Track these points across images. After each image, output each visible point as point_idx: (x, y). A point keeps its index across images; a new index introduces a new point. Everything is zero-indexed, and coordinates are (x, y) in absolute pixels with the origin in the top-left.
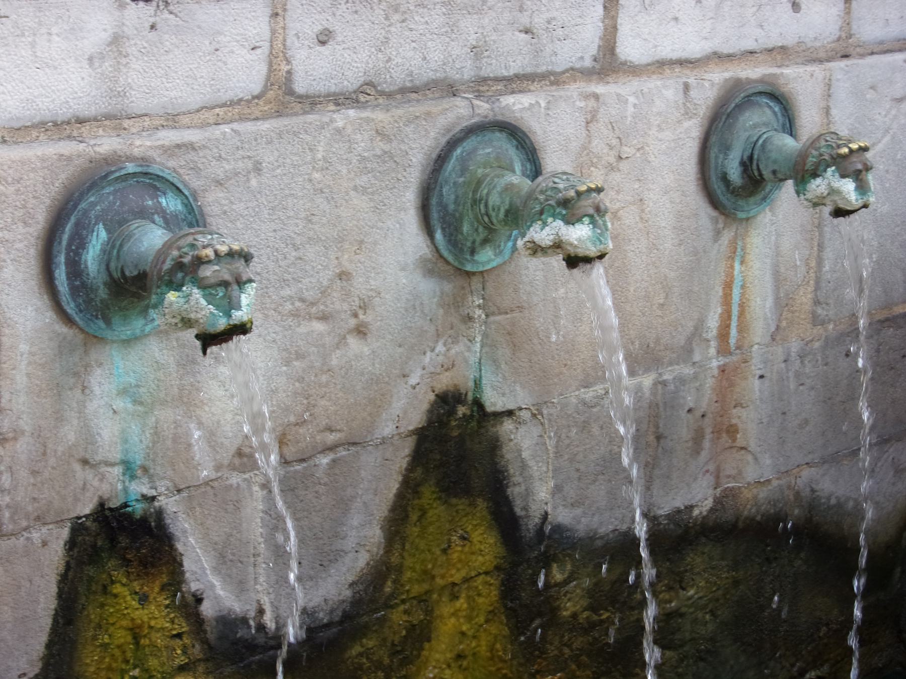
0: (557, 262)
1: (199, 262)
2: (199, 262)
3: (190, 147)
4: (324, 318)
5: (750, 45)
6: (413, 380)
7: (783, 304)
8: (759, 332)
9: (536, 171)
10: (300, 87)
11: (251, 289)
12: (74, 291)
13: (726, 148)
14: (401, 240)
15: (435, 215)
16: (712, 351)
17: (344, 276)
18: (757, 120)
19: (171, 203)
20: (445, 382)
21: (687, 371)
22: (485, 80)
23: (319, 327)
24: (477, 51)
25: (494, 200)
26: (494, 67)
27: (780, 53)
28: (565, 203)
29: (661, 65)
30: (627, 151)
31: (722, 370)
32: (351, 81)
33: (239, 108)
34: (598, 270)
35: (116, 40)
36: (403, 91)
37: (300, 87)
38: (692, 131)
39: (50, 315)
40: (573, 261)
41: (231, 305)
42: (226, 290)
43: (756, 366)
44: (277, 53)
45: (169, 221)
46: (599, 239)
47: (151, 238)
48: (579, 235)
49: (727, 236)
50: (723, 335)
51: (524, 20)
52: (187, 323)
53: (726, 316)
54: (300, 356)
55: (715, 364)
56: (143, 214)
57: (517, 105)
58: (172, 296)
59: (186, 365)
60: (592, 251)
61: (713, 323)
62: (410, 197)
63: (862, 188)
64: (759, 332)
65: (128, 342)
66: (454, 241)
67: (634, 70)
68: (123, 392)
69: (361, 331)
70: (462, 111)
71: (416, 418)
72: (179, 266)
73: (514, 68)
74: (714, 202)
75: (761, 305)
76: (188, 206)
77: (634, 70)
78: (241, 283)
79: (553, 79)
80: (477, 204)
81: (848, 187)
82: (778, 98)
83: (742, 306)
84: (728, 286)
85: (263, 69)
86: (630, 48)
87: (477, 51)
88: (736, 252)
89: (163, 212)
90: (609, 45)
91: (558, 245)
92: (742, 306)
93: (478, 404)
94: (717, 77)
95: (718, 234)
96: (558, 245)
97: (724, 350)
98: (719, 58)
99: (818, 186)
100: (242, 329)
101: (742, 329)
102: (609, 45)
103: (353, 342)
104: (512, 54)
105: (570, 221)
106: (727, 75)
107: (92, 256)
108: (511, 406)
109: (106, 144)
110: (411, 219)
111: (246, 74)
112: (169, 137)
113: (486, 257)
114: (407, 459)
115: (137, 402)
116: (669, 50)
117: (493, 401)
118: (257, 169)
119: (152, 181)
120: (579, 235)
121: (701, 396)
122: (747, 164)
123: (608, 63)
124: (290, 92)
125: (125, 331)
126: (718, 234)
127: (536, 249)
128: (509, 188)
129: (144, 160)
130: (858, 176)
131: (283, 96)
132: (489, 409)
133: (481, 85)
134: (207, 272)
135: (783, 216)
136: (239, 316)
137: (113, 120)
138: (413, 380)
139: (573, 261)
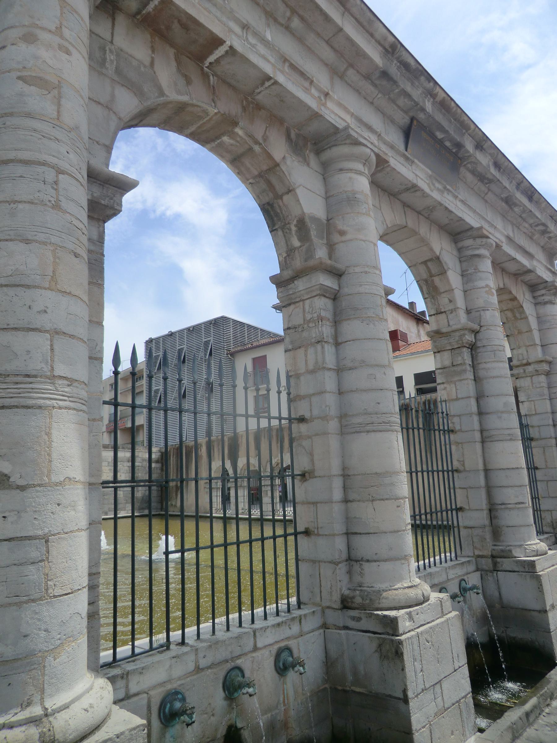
0: (248, 695)
1: (186, 710)
2: (186, 710)
3: (183, 684)
4: (206, 714)
5: (282, 638)
6: (223, 724)
7: (296, 692)
8: (291, 699)
9: (243, 676)
10: (201, 667)
11: (195, 714)
12: (164, 717)
13: (279, 661)
14: (220, 694)
15: (225, 687)
16: (282, 706)
17: (210, 704)
18: (285, 655)
19: (180, 696)
20: (229, 723)
21: (277, 711)
22: (233, 658)
23: (206, 716)
24: (231, 652)
25: (236, 683)
26: (235, 654)
27: (288, 639)
28: (248, 684)
29: (265, 647)
30: (260, 666)
31: (285, 710)
32: (209, 664)
33: (191, 674)
34: (255, 697)
35: (170, 666)
36: (218, 663)
37: (201, 667)
38: (272, 659)
39: (159, 723)
40: (251, 695)
41: (191, 718)
42: (190, 716)
43: (292, 707)
44: (197, 662)
45: (180, 700)
46: (254, 691)
47: (178, 705)
48: (251, 690)
49: (282, 679)
50: (284, 702)
51: (239, 644)
52: (184, 722)
53: (284, 697)
54: (202, 723)
55: (283, 708)
56: (175, 700)
57: (239, 662)
58: (182, 717)
59: (182, 729)
60: (253, 693)
61: (281, 699)
62: (221, 681)
63: (304, 668)
64: (291, 699)
65: (172, 726)
66: (229, 693)
67: (261, 649)
68: (171, 737)
69: (213, 715)
70: (229, 666)
71: (224, 732)
72: (183, 711)
73: (238, 654)
74: (279, 673)
75: (291, 693)
76: (183, 696)
77: (261, 649)
78: (193, 713)
79: (245, 654)
80: (233, 686)
81: (301, 668)
82: (288, 649)
83: (287, 694)
84: (284, 690)
85: (194, 665)
86: (259, 645)
87: (231, 652)
88: (284, 683)
89: (178, 698)
90: (255, 645)
91: (247, 693)
92: (287, 694)
93: (236, 727)
94: (276, 647)
95: (280, 680)
96: (247, 693)
97: (284, 705)
98: (276, 642)
99: (296, 669)
100: (194, 722)
101: (287, 700)
102: (255, 645)
103: (212, 718)
104: (238, 652)
105: (249, 688)
106: (278, 646)
107: (167, 710)
108: (445, 310)
109: (169, 687)
110: (221, 689)
111: (191, 666)
112: (179, 683)
113: (236, 695)
114: (157, 39)
115: (174, 738)
116: (267, 643)
117: (239, 725)
118: (194, 686)
119: (177, 693)
120: (251, 690)
121: (281, 717)
122: (284, 664)
123: (256, 649)
124: (199, 668)
125: (173, 724)
126: (280, 680)
127: (243, 694)
128: (238, 681)
129: (175, 689)
130: (303, 666)
131: (198, 669)
132: (238, 727)
133: (233, 659)
134: (188, 712)
135: (291, 675)
136: (193, 720)
137: (169, 681)
138: (223, 724)
139: (251, 695)
